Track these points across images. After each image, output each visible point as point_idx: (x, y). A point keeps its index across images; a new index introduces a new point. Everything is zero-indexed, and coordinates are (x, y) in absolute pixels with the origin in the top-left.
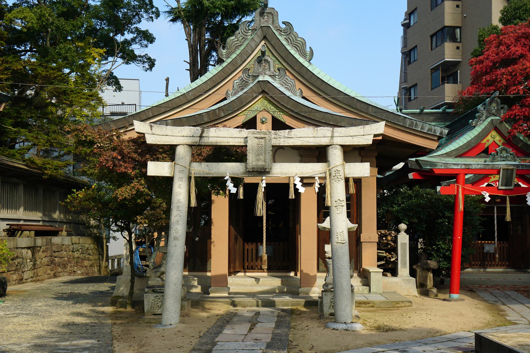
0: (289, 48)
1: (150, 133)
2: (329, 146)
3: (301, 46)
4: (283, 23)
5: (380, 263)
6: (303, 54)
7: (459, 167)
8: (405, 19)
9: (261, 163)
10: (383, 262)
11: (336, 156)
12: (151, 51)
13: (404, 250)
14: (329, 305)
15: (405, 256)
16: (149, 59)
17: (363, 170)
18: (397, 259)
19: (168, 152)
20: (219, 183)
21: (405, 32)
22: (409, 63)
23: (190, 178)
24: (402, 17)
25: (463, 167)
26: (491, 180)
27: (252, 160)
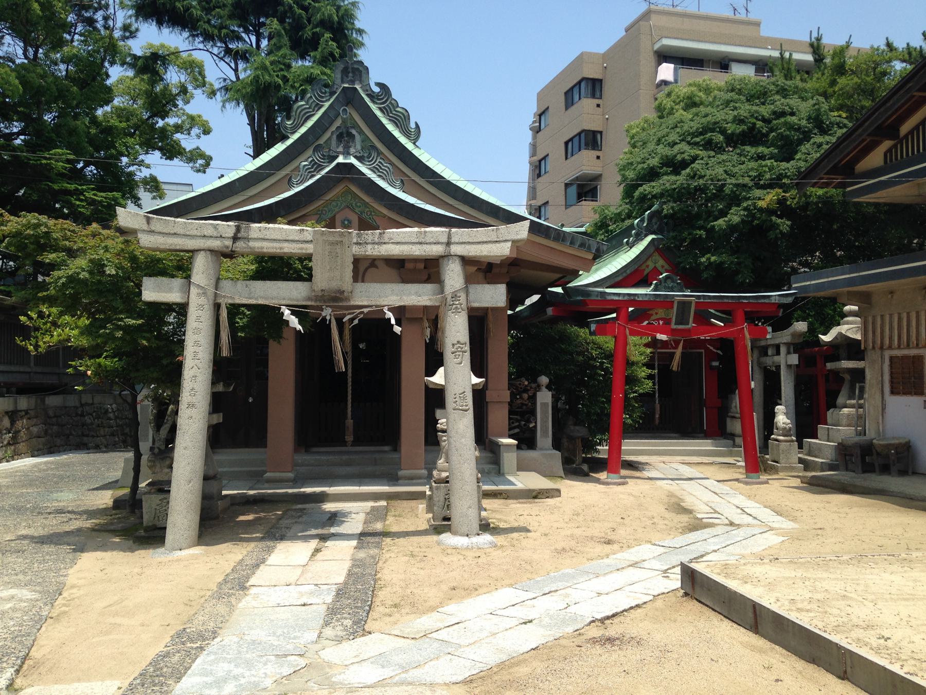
0: (384, 121)
1: (146, 228)
2: (442, 257)
3: (402, 120)
4: (378, 84)
5: (512, 432)
6: (406, 133)
7: (621, 298)
8: (534, 122)
9: (335, 285)
10: (517, 431)
11: (453, 276)
12: (206, 144)
13: (545, 413)
14: (441, 503)
15: (547, 421)
16: (202, 156)
17: (494, 296)
18: (535, 427)
19: (178, 266)
20: (268, 315)
21: (534, 138)
22: (539, 175)
23: (217, 307)
24: (529, 117)
25: (626, 298)
26: (653, 318)
27: (323, 279)
